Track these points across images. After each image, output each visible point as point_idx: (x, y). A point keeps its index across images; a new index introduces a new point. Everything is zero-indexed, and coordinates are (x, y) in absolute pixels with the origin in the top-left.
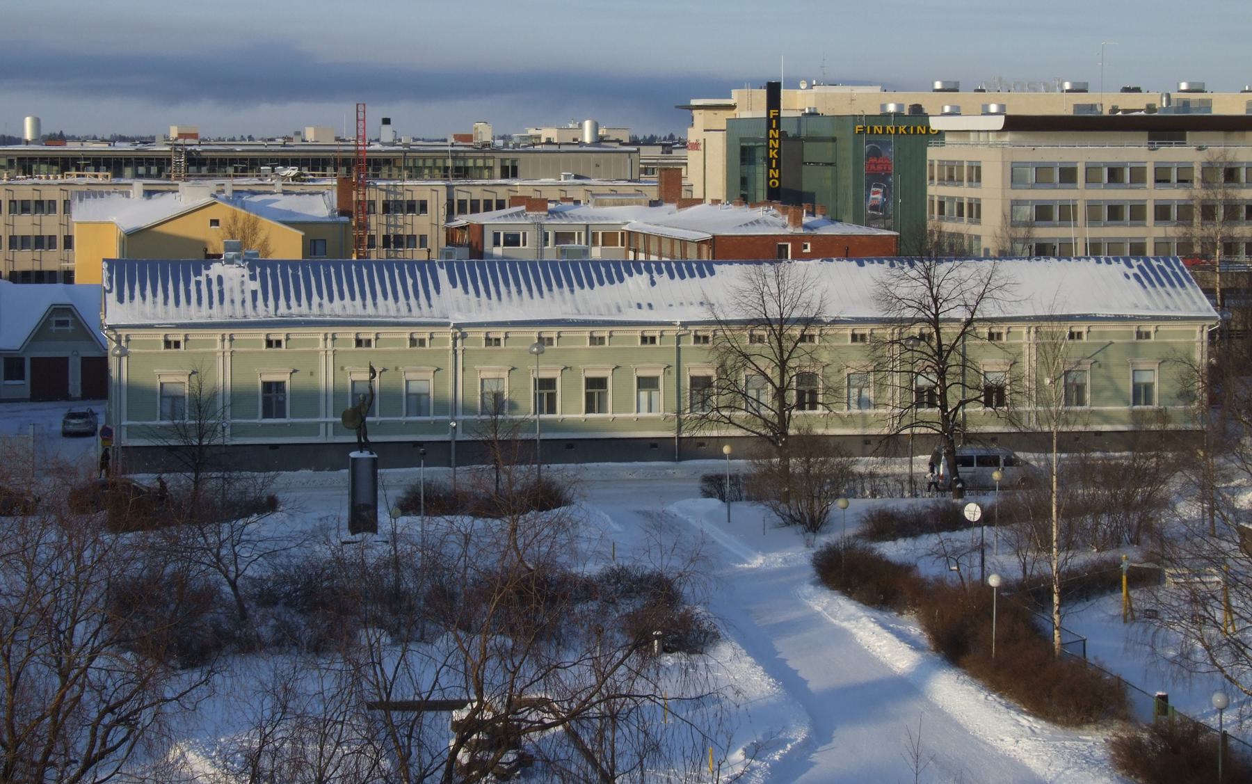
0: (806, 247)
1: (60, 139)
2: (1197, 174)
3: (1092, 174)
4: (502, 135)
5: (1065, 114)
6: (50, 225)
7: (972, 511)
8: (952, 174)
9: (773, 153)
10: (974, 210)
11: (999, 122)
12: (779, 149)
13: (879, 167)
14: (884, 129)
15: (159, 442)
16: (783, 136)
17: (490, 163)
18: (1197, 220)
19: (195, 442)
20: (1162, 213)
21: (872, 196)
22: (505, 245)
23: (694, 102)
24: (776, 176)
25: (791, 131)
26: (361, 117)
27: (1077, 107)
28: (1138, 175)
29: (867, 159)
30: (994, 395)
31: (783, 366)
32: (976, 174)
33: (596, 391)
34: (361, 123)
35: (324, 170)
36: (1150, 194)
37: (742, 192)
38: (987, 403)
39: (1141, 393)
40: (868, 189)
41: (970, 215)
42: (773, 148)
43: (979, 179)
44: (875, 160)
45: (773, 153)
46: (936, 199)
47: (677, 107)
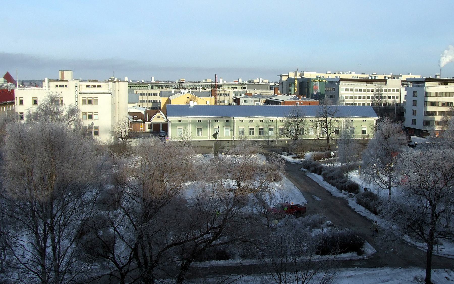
1: (158, 81)
4: (164, 80)
7: (332, 154)
15: (178, 140)
19: (184, 140)
23: (283, 75)
30: (337, 132)
31: (297, 126)
38: (336, 134)
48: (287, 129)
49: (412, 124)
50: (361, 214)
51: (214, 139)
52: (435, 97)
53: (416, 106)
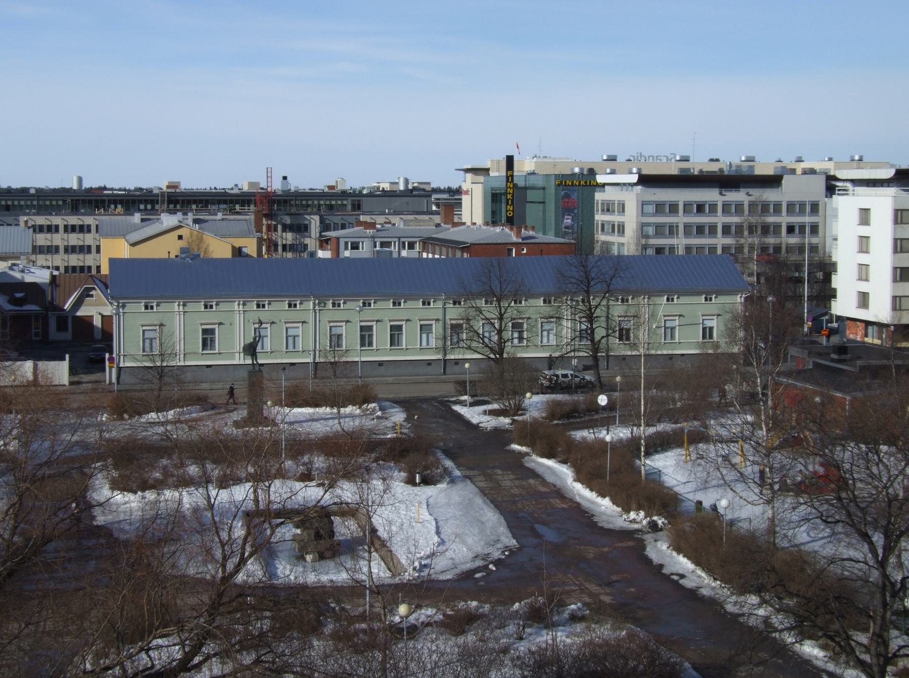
0: (523, 250)
2: (746, 207)
3: (687, 206)
5: (673, 173)
6: (89, 239)
8: (608, 208)
9: (509, 196)
10: (621, 229)
11: (634, 178)
12: (513, 194)
13: (570, 204)
14: (573, 182)
15: (139, 364)
16: (515, 186)
17: (345, 202)
18: (746, 233)
19: (158, 364)
20: (726, 230)
21: (565, 221)
22: (352, 249)
24: (511, 209)
25: (521, 183)
26: (269, 175)
27: (681, 170)
28: (713, 208)
29: (563, 199)
32: (622, 208)
33: (209, 336)
34: (269, 179)
35: (249, 206)
36: (720, 219)
37: (493, 219)
39: (707, 332)
40: (563, 217)
41: (619, 231)
42: (510, 193)
43: (623, 211)
44: (566, 200)
45: (509, 196)
46: (600, 223)
47: (456, 170)
48: (472, 327)
49: (859, 307)
50: (681, 582)
51: (249, 361)
52: (900, 297)
53: (867, 252)
